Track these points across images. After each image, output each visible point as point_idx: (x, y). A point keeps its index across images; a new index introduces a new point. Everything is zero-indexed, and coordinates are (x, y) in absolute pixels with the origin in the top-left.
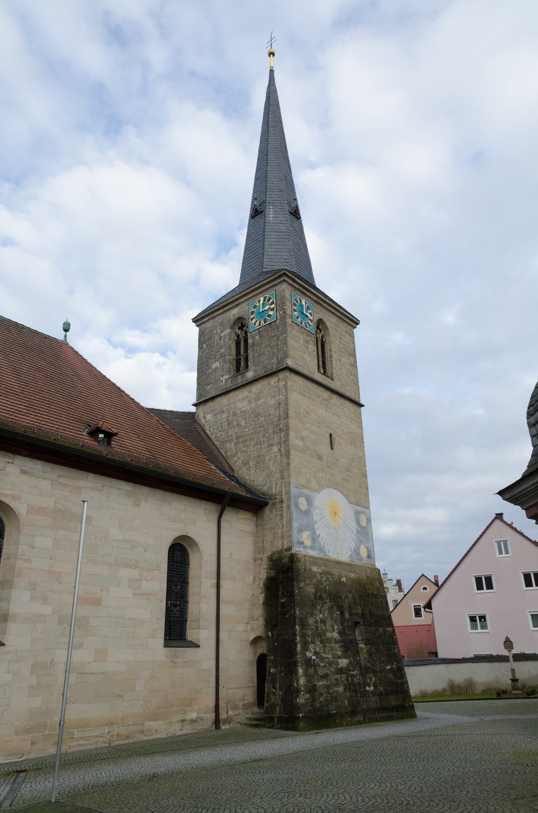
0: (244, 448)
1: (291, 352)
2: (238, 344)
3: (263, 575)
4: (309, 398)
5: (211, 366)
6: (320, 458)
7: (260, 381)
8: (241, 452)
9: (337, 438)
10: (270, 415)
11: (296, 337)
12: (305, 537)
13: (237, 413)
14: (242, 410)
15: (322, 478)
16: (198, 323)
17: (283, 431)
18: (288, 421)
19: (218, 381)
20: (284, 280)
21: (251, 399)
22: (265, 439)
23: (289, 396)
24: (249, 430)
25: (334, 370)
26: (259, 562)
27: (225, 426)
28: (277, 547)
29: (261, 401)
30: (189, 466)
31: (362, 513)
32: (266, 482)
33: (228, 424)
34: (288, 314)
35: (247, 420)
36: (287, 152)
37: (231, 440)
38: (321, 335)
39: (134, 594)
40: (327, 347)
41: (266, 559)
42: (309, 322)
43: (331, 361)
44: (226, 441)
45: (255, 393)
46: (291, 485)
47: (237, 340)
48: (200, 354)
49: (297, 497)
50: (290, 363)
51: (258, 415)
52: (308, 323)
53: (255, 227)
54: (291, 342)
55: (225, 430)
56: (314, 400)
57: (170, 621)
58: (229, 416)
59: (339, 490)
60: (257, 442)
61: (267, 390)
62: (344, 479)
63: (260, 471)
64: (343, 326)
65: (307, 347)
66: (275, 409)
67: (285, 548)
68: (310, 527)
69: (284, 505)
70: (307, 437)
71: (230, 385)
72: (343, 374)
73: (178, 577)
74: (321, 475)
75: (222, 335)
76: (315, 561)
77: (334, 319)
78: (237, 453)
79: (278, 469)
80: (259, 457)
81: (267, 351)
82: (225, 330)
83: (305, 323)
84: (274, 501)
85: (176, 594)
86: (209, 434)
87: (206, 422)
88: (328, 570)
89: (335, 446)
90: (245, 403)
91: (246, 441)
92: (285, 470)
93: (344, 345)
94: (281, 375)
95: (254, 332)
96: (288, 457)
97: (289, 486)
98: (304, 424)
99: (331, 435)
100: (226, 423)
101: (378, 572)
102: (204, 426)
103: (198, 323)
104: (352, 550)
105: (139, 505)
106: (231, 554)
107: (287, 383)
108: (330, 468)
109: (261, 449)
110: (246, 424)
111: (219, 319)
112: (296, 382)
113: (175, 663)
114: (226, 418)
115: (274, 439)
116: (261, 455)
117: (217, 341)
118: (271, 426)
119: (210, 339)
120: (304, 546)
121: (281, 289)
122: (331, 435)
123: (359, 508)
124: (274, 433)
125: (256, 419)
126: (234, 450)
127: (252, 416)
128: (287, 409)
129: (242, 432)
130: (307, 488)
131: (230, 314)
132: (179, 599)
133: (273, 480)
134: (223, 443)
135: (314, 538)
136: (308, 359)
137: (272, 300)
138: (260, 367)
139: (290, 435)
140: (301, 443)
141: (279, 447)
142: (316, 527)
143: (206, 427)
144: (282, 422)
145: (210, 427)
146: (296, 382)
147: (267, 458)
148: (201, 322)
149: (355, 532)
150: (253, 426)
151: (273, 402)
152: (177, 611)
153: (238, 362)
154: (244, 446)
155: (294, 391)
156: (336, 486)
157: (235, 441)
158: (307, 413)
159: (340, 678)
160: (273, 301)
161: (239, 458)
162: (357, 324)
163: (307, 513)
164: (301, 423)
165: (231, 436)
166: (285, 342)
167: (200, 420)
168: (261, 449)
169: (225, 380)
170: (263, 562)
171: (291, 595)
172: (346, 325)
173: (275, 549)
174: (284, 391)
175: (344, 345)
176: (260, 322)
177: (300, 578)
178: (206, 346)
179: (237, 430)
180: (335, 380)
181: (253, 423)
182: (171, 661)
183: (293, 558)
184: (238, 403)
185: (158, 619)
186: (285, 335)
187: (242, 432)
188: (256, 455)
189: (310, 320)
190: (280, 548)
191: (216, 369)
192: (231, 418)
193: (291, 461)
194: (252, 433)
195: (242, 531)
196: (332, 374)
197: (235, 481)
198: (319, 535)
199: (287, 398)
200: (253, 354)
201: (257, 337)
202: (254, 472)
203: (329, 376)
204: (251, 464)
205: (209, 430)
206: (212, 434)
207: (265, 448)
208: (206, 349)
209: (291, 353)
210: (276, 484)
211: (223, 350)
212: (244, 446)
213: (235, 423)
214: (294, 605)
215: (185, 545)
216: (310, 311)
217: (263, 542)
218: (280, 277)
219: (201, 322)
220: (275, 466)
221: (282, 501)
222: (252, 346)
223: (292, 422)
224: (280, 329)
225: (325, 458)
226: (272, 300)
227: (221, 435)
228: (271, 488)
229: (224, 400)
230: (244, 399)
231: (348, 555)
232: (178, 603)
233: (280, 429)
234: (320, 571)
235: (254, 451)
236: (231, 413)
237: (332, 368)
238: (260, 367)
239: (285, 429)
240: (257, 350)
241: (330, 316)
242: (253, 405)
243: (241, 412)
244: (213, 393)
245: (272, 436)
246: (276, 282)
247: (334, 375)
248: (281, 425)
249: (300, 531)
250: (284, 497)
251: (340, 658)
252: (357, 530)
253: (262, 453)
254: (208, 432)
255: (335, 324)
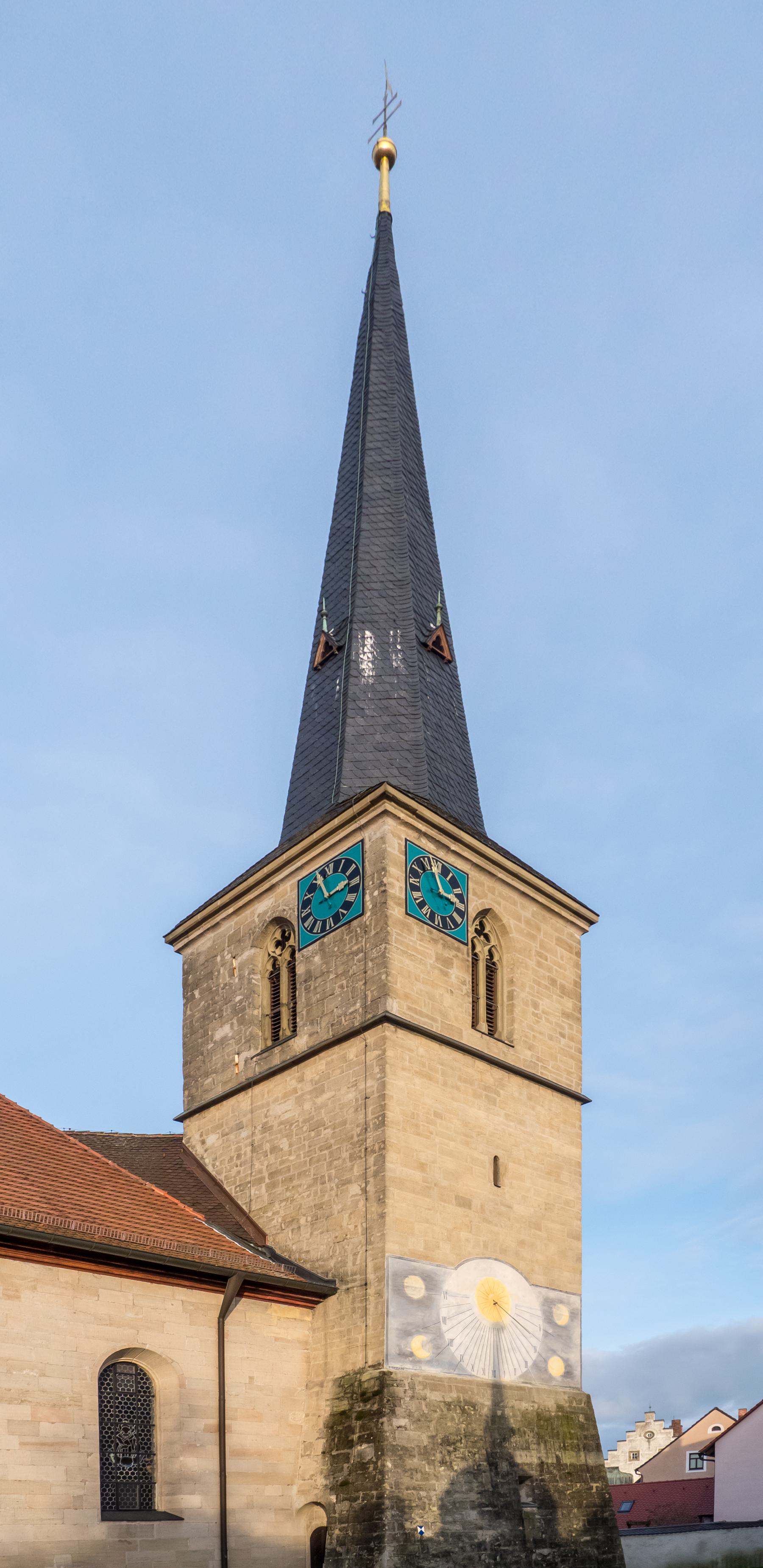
0: (288, 1194)
1: (399, 984)
2: (274, 978)
3: (325, 1410)
4: (445, 1084)
5: (212, 1036)
6: (464, 1203)
7: (323, 1054)
8: (281, 1201)
9: (511, 1166)
10: (344, 1123)
11: (416, 950)
12: (418, 1345)
13: (272, 1127)
14: (283, 1118)
15: (467, 1240)
16: (180, 945)
17: (373, 1151)
18: (384, 1131)
19: (228, 1064)
20: (385, 812)
21: (303, 1095)
22: (333, 1171)
23: (390, 1080)
24: (298, 1156)
25: (516, 1026)
26: (316, 1389)
27: (245, 1154)
28: (354, 1364)
29: (326, 1096)
30: (151, 1229)
31: (561, 1302)
32: (334, 1252)
33: (253, 1151)
34: (394, 897)
35: (294, 1139)
36: (423, 473)
37: (262, 1180)
38: (487, 948)
39: (22, 1444)
40: (503, 976)
41: (330, 1384)
42: (455, 915)
43: (512, 1006)
44: (250, 1182)
45: (311, 1081)
46: (387, 1254)
47: (272, 973)
48: (189, 1012)
49: (401, 1276)
50: (395, 1007)
51: (317, 1126)
52: (451, 917)
53: (321, 694)
54: (398, 961)
55: (245, 1162)
56: (458, 1088)
57: (117, 1483)
58: (253, 1134)
59: (506, 1263)
60: (315, 1180)
61: (339, 1071)
62: (522, 1243)
63: (322, 1233)
64: (554, 929)
65: (446, 974)
66: (356, 1110)
67: (370, 1363)
68: (432, 1329)
69: (371, 1291)
70: (433, 1162)
71: (257, 1070)
72: (541, 1033)
73: (129, 1417)
74: (464, 1235)
75: (235, 963)
76: (434, 1384)
77: (530, 910)
78: (271, 1203)
79: (359, 1228)
80: (319, 1206)
81: (342, 987)
82: (243, 951)
83: (443, 919)
84: (350, 1286)
85: (127, 1442)
86: (213, 1173)
87: (206, 1151)
88: (467, 1398)
89: (504, 1180)
90: (290, 1104)
91: (291, 1179)
92: (374, 1227)
93: (550, 970)
94: (371, 1036)
95: (310, 948)
96: (381, 1202)
97: (383, 1256)
98: (427, 1138)
99: (496, 1158)
100: (249, 1148)
101: (584, 1399)
102: (202, 1158)
103: (180, 945)
104: (530, 1363)
105: (18, 1298)
106: (251, 1378)
107: (384, 1051)
108: (489, 1222)
109: (323, 1191)
110: (290, 1145)
111: (228, 927)
112: (411, 1050)
113: (129, 1543)
114: (247, 1138)
115: (352, 1169)
116: (322, 1204)
117: (224, 979)
118: (345, 1145)
119: (210, 975)
120: (413, 1360)
121: (378, 835)
122: (496, 1158)
123: (553, 1294)
124: (352, 1158)
125: (313, 1134)
126: (266, 1198)
127: (305, 1129)
128: (383, 1107)
129: (282, 1162)
130: (426, 1258)
131: (253, 913)
132: (132, 1451)
133: (349, 1248)
134: (242, 1186)
135: (440, 1347)
136: (448, 1000)
137: (354, 866)
138: (324, 1024)
139: (388, 1159)
140: (418, 1175)
141: (363, 1185)
142: (444, 1328)
143: (207, 1161)
144: (371, 1135)
145: (215, 1159)
146: (411, 1050)
147: (336, 1208)
148: (186, 941)
149: (540, 1335)
150: (307, 1149)
151: (351, 1096)
152: (130, 1469)
153: (276, 1018)
154: (287, 1189)
155: (403, 1069)
156: (500, 1254)
157: (267, 1181)
158: (437, 1115)
159: (477, 1557)
160: (357, 869)
161: (277, 1213)
162: (591, 923)
163: (425, 1303)
164: (418, 1134)
165: (260, 1171)
166: (383, 962)
167: (193, 1147)
168: (323, 1191)
169: (242, 1062)
170: (324, 1389)
171: (375, 1438)
172: (560, 923)
173: (349, 1368)
174: (377, 1070)
175: (550, 970)
176: (324, 922)
177: (398, 1410)
178: (200, 993)
179: (272, 1158)
180: (518, 1047)
181: (307, 1143)
182: (120, 1541)
183: (384, 1380)
184: (272, 1106)
185: (84, 1481)
186: (384, 945)
187: (282, 1162)
188: (312, 1204)
189: (458, 910)
190: (360, 1364)
191: (224, 1040)
192: (258, 1137)
193: (388, 1210)
194: (305, 1162)
195: (276, 1339)
196: (511, 1033)
197: (269, 1255)
198: (452, 1340)
199: (383, 1085)
200: (308, 999)
201: (317, 959)
202: (308, 1235)
203: (504, 1038)
204: (302, 1221)
205: (213, 1165)
206: (219, 1173)
207: (332, 1189)
208: (201, 999)
209: (398, 986)
210: (355, 1255)
211: (238, 998)
212: (287, 1189)
213: (267, 1147)
214: (383, 1454)
215: (142, 1364)
216: (458, 891)
217: (326, 1356)
218: (374, 803)
219: (186, 941)
220: (353, 1220)
221: (366, 1284)
222: (305, 981)
223: (393, 1134)
224: (373, 933)
225: (476, 1203)
226: (354, 866)
227: (239, 1172)
228: (344, 1263)
229: (243, 1100)
230: (286, 1096)
231: (519, 1373)
232: (133, 1457)
233: (366, 1149)
234: (448, 1400)
235: (308, 1196)
236: (259, 1128)
237: (513, 1021)
238: (324, 1024)
239: (377, 1147)
240: (315, 988)
241: (515, 903)
242: (307, 1106)
243: (281, 1123)
244: (219, 1091)
245: (349, 1164)
246: (363, 821)
247: (515, 1037)
248: (368, 1141)
249: (407, 1333)
250: (371, 1277)
251: (481, 1528)
252: (545, 1331)
253: (326, 1198)
254: (210, 1169)
255: (528, 923)
